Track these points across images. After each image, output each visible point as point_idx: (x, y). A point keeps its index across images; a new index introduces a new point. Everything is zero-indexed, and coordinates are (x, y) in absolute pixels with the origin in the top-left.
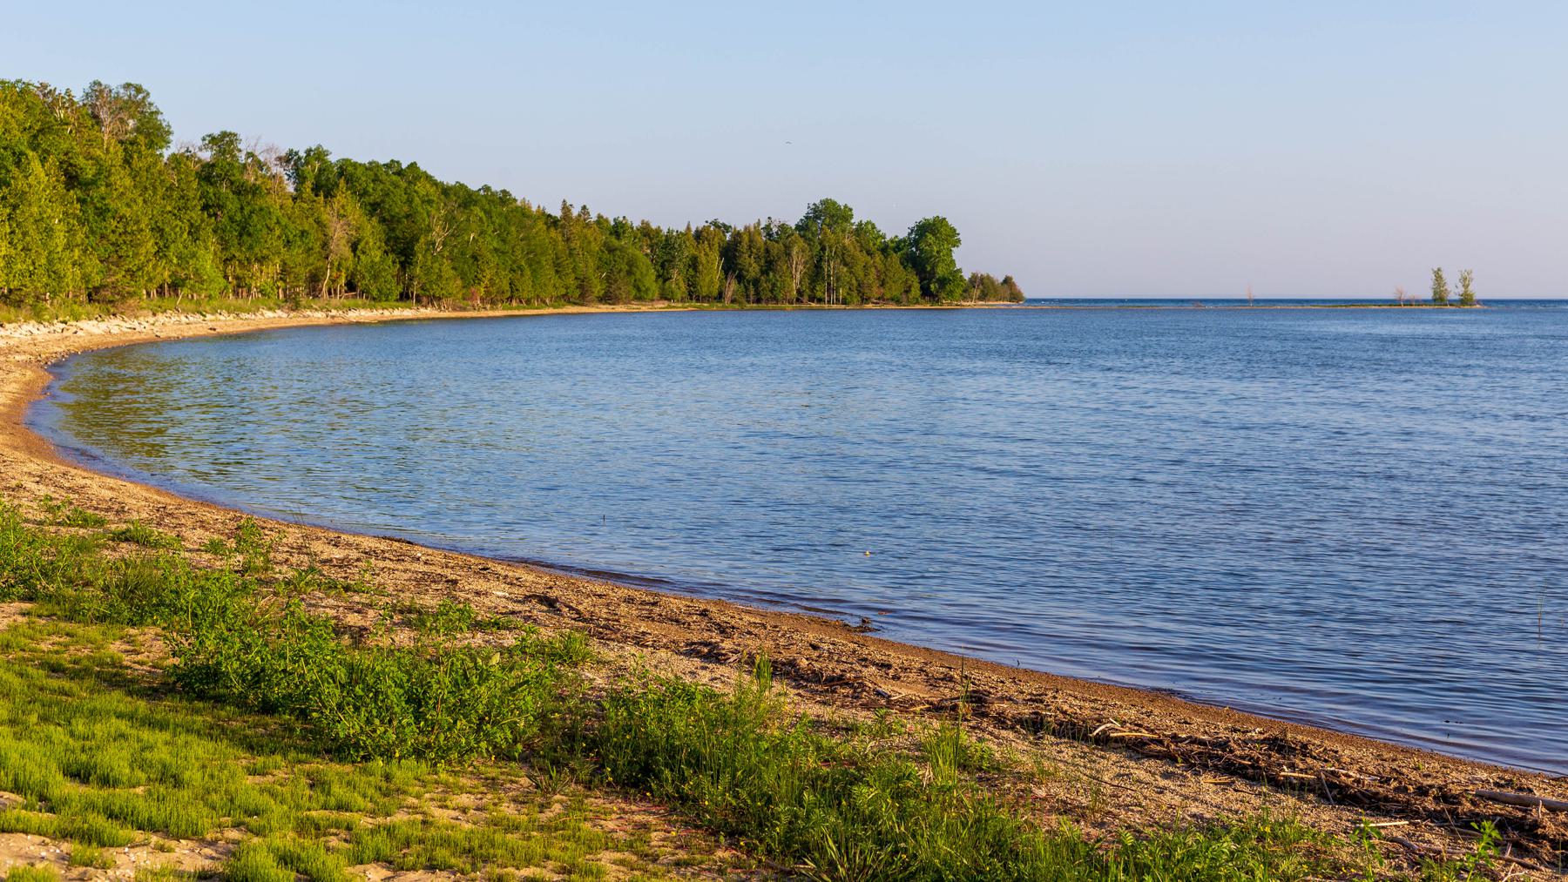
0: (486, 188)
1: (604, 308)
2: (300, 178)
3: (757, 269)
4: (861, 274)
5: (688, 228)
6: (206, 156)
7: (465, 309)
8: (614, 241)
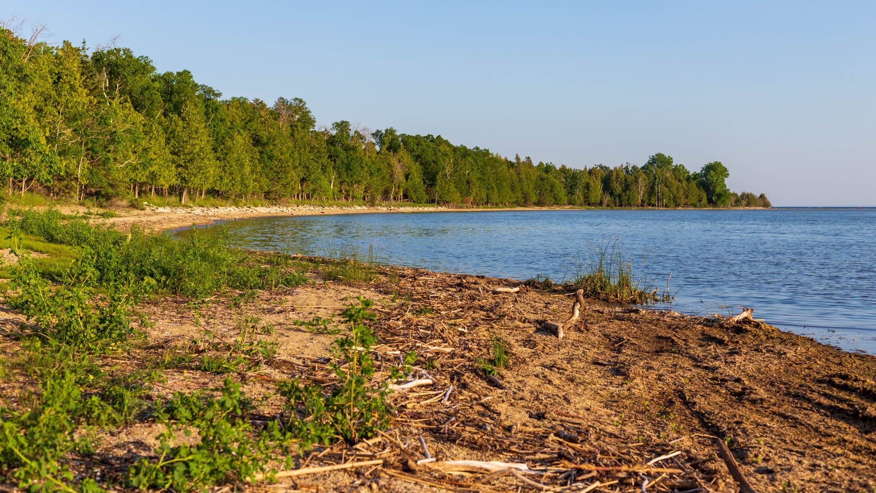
0: (477, 148)
1: (537, 208)
2: (382, 143)
3: (620, 189)
4: (675, 191)
5: (586, 168)
6: (334, 132)
7: (462, 208)
8: (545, 175)
